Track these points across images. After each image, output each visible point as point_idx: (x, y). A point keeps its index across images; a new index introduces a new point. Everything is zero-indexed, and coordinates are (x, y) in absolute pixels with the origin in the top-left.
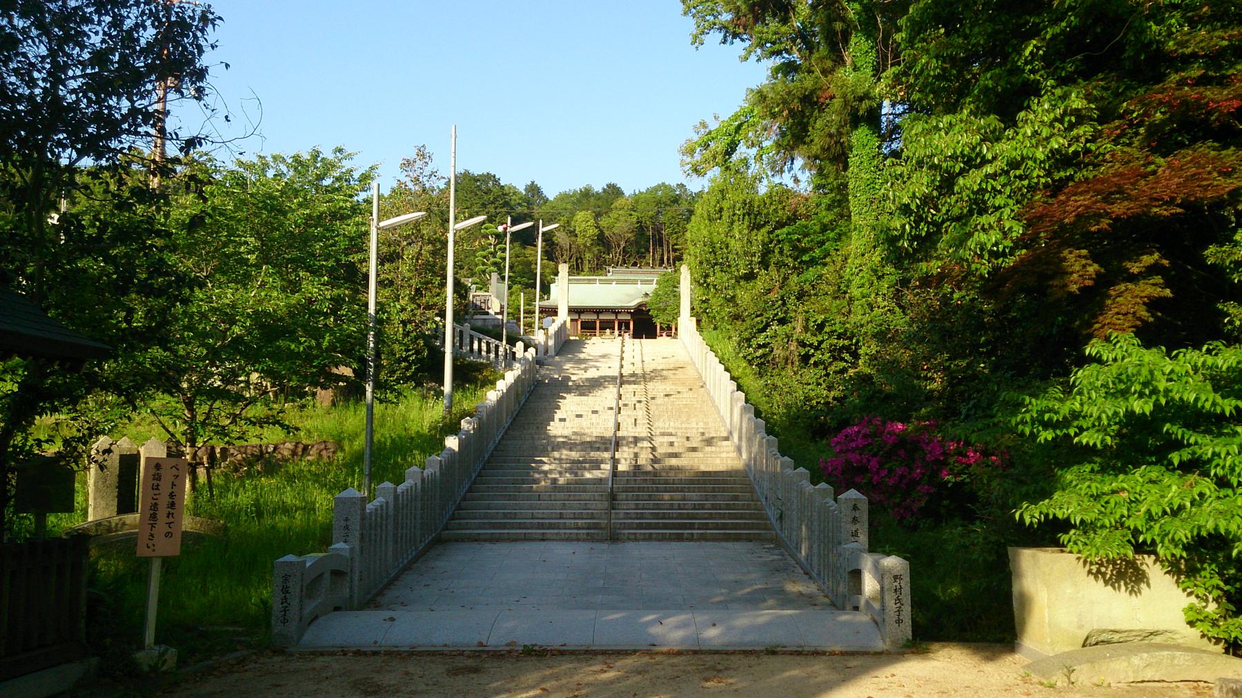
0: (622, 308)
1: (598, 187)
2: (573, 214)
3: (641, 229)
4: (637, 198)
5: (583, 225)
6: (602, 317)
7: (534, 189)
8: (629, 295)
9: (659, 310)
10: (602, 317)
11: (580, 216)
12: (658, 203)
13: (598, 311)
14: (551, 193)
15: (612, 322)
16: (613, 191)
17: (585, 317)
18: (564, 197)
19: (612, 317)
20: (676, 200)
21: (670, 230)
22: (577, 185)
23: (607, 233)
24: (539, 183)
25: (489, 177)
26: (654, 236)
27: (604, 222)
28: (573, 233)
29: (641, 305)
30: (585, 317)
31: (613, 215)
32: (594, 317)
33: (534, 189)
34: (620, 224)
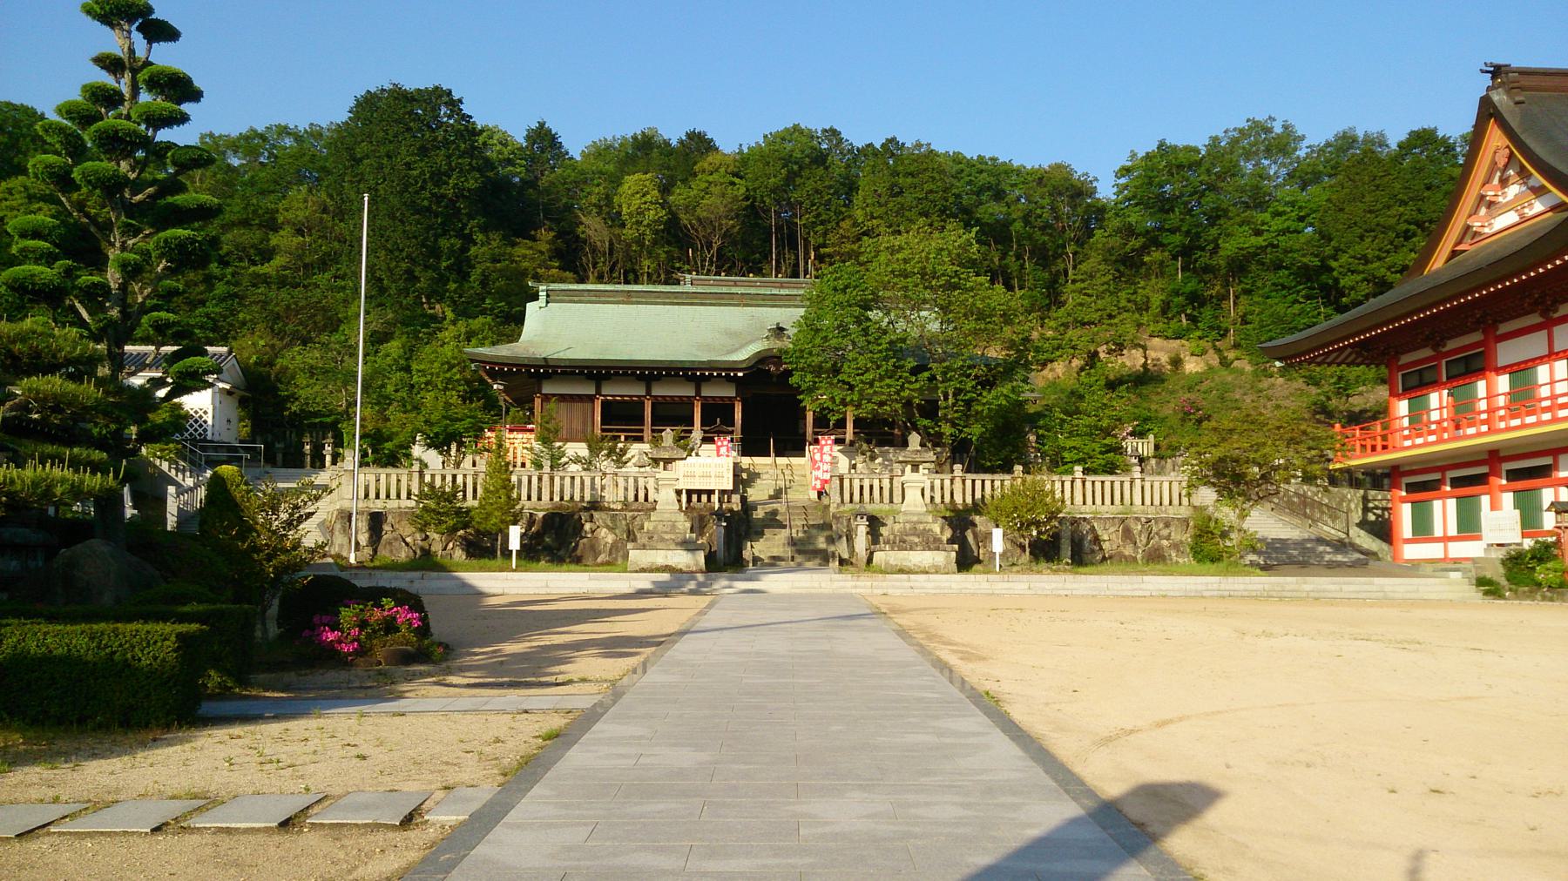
0: (712, 366)
1: (673, 133)
2: (616, 181)
3: (752, 212)
4: (741, 165)
5: (636, 202)
6: (659, 391)
7: (543, 138)
8: (729, 333)
9: (817, 371)
10: (659, 391)
11: (631, 182)
12: (787, 161)
13: (649, 373)
14: (575, 144)
15: (688, 403)
16: (699, 144)
17: (613, 391)
18: (601, 152)
19: (687, 391)
20: (820, 159)
21: (810, 217)
22: (622, 127)
23: (684, 219)
24: (553, 126)
25: (440, 97)
26: (779, 228)
27: (678, 197)
28: (615, 220)
29: (762, 359)
30: (613, 391)
31: (698, 184)
32: (638, 390)
33: (543, 138)
34: (708, 200)
